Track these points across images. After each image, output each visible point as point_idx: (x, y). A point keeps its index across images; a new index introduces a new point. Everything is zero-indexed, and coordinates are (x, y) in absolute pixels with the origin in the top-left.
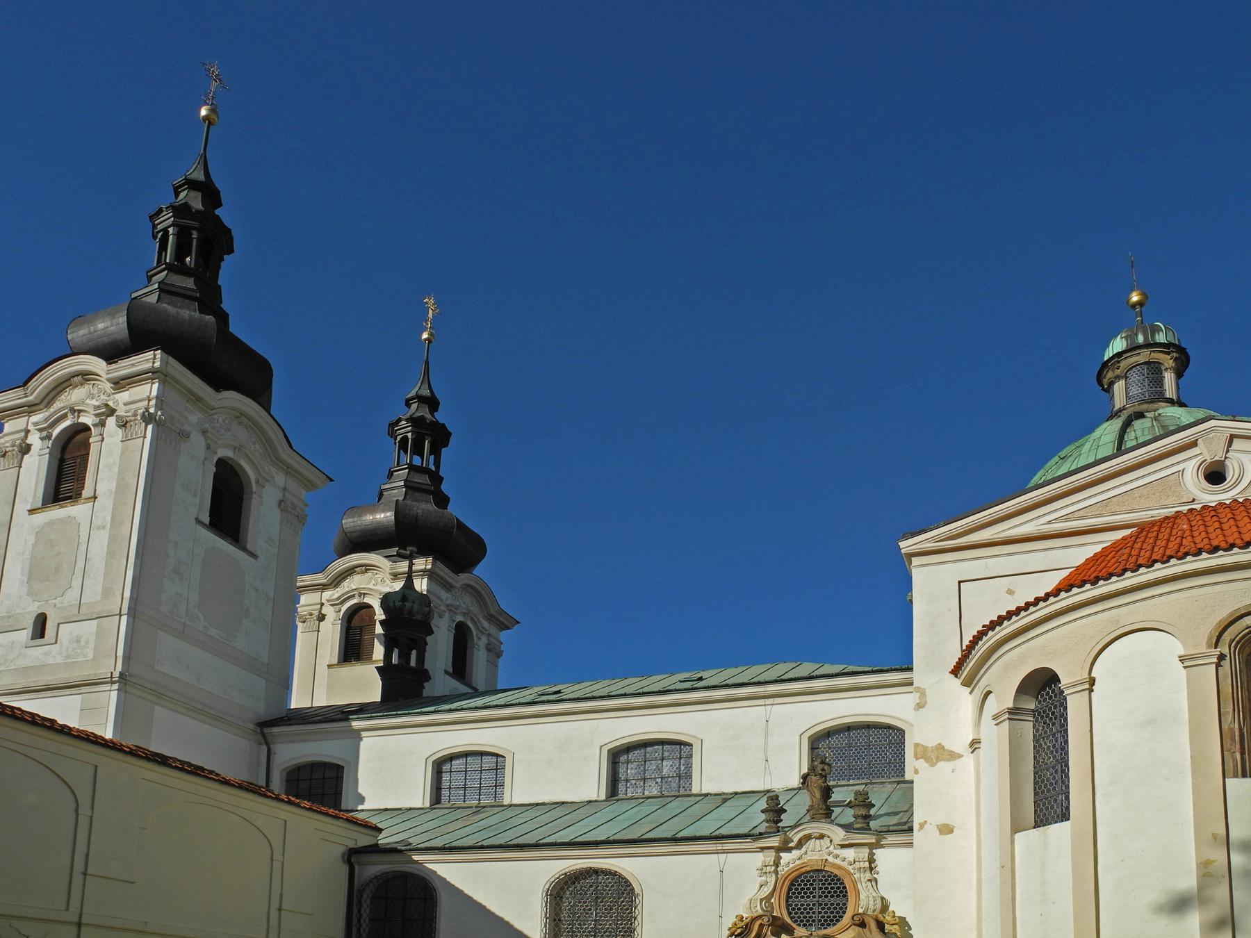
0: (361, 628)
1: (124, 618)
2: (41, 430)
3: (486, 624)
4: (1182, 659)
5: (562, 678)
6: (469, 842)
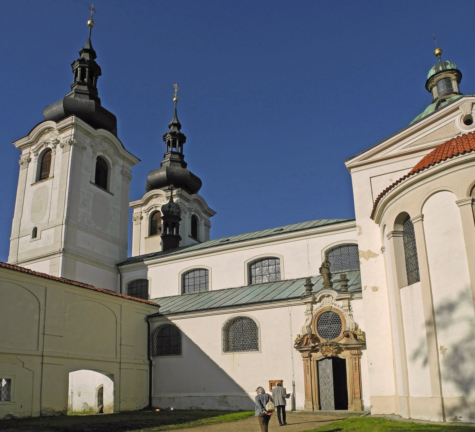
0: (156, 221)
1: (64, 226)
2: (34, 152)
3: (204, 215)
5: (229, 236)
6: (194, 308)
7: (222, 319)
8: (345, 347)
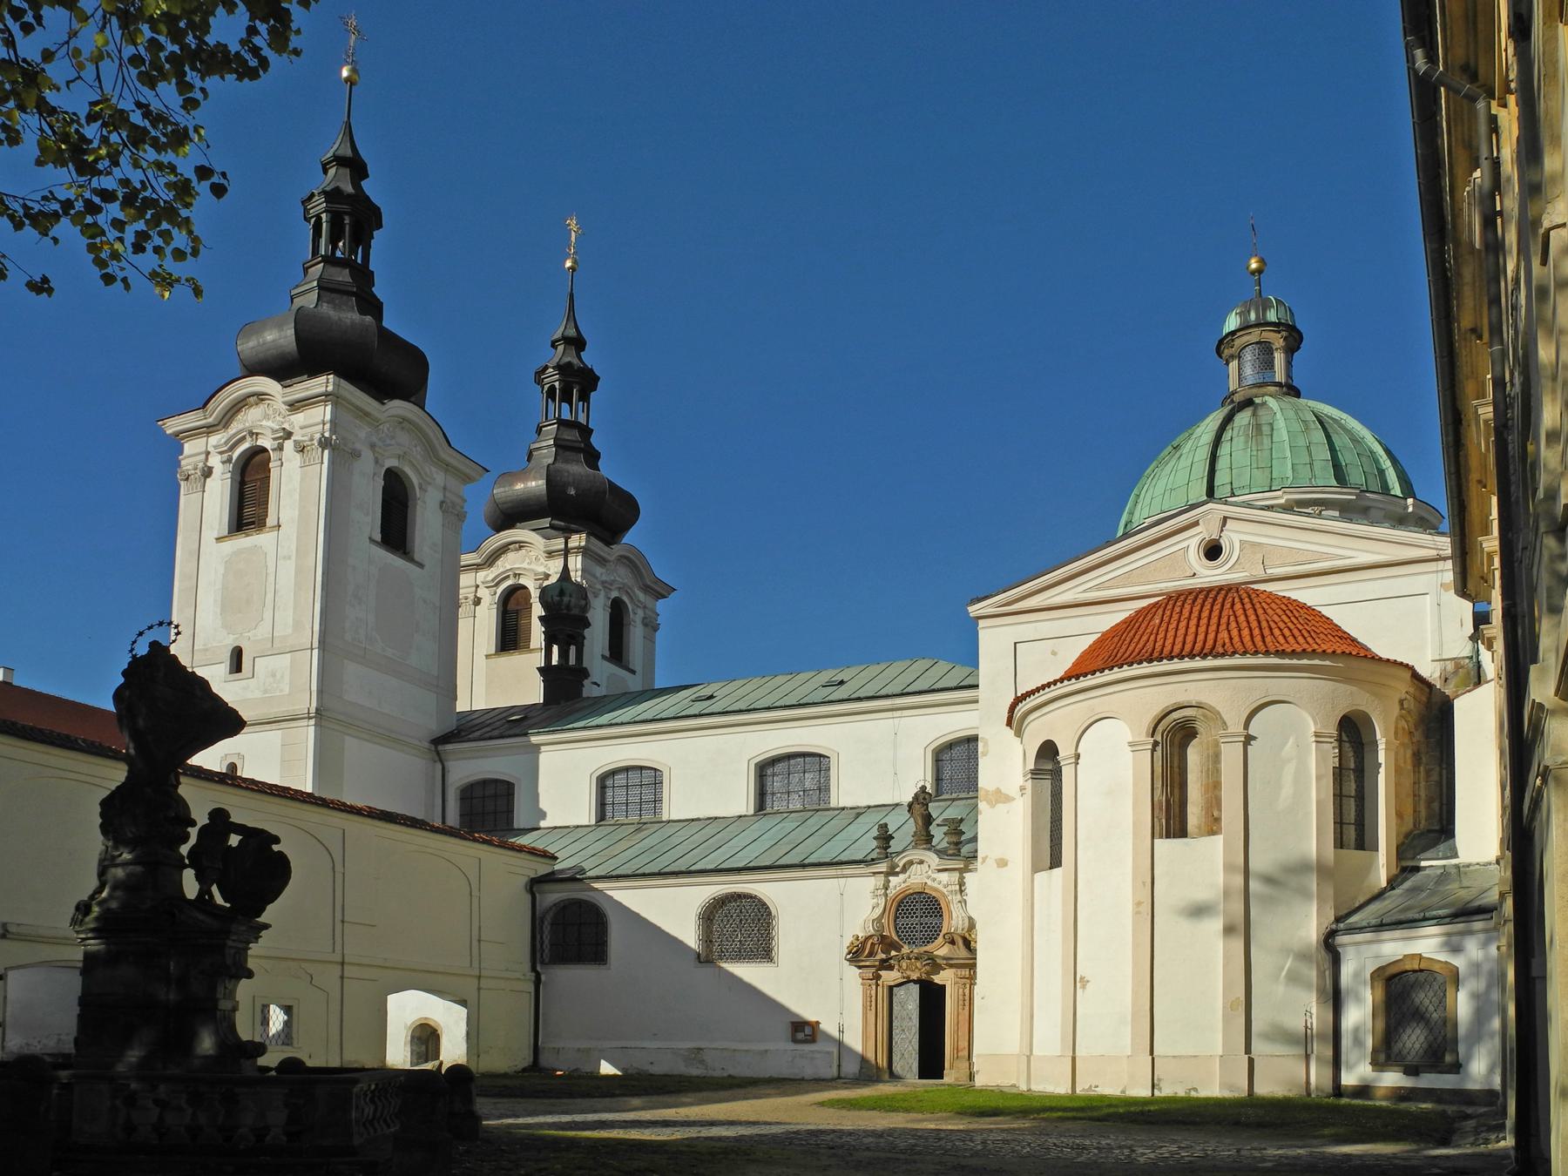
0: (517, 612)
1: (316, 652)
3: (641, 596)
4: (1131, 744)
7: (702, 893)
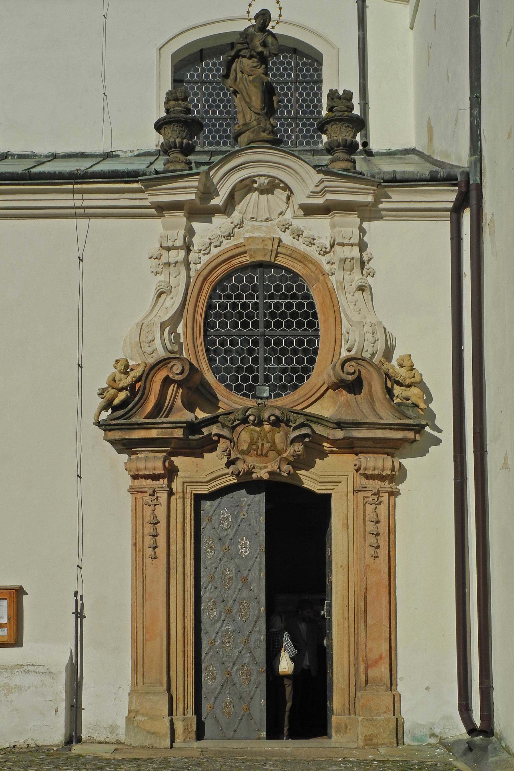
7: (428, 355)
8: (340, 434)
